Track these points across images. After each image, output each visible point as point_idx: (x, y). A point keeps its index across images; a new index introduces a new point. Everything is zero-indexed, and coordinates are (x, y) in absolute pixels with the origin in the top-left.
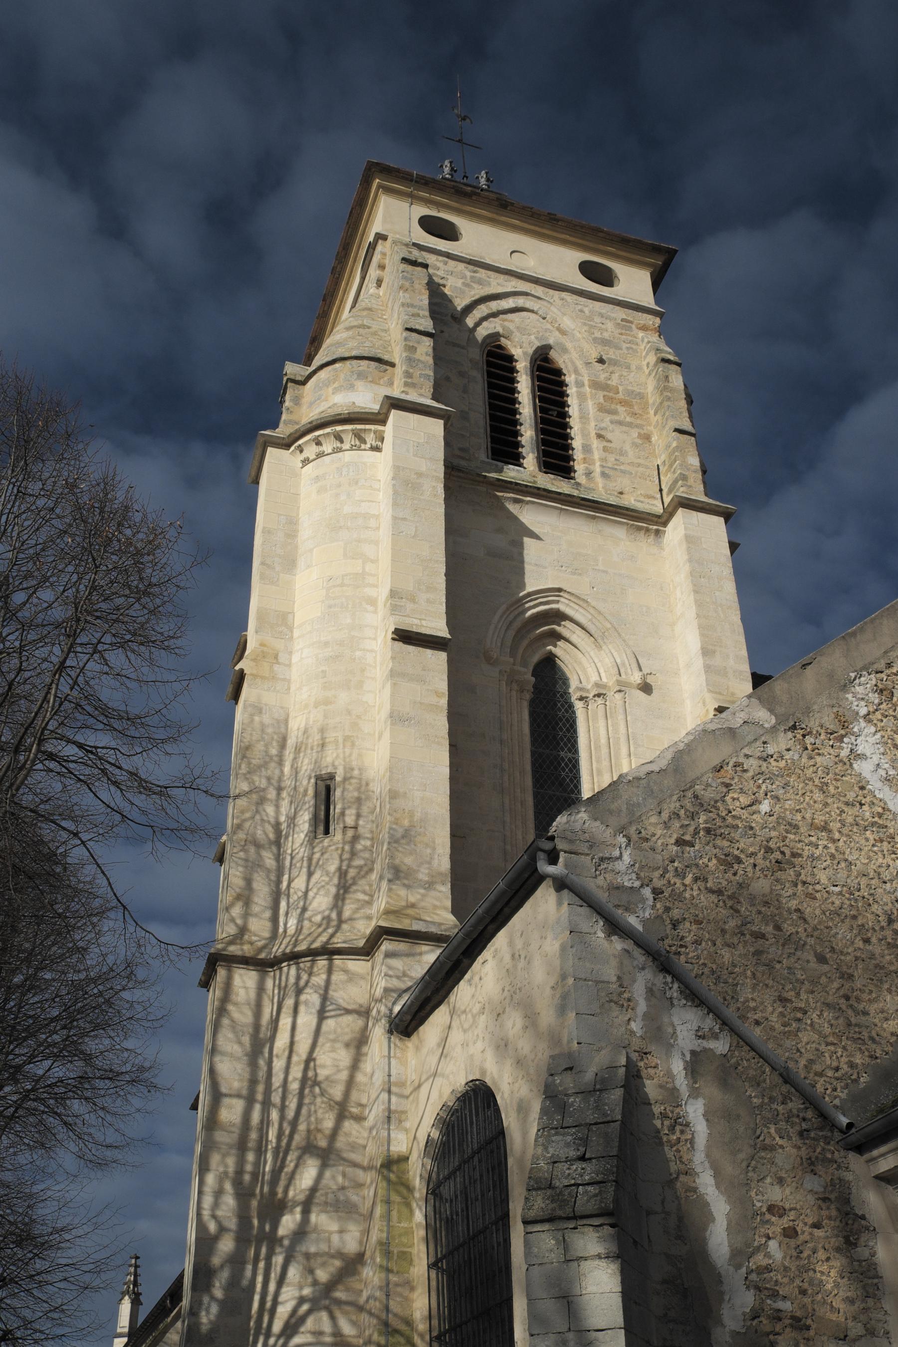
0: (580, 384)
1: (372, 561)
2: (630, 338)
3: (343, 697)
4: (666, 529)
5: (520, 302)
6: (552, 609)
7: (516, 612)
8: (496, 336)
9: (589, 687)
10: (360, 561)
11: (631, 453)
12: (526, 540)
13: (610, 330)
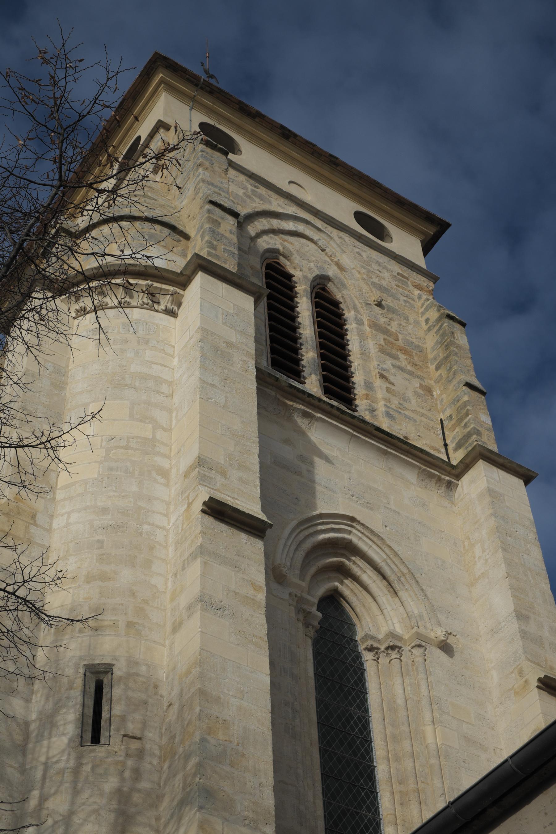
0: (360, 322)
1: (165, 430)
2: (406, 293)
3: (126, 576)
4: (460, 482)
5: (301, 228)
6: (344, 539)
7: (307, 533)
8: (274, 252)
9: (380, 636)
10: (150, 426)
11: (413, 402)
12: (317, 460)
13: (387, 279)
